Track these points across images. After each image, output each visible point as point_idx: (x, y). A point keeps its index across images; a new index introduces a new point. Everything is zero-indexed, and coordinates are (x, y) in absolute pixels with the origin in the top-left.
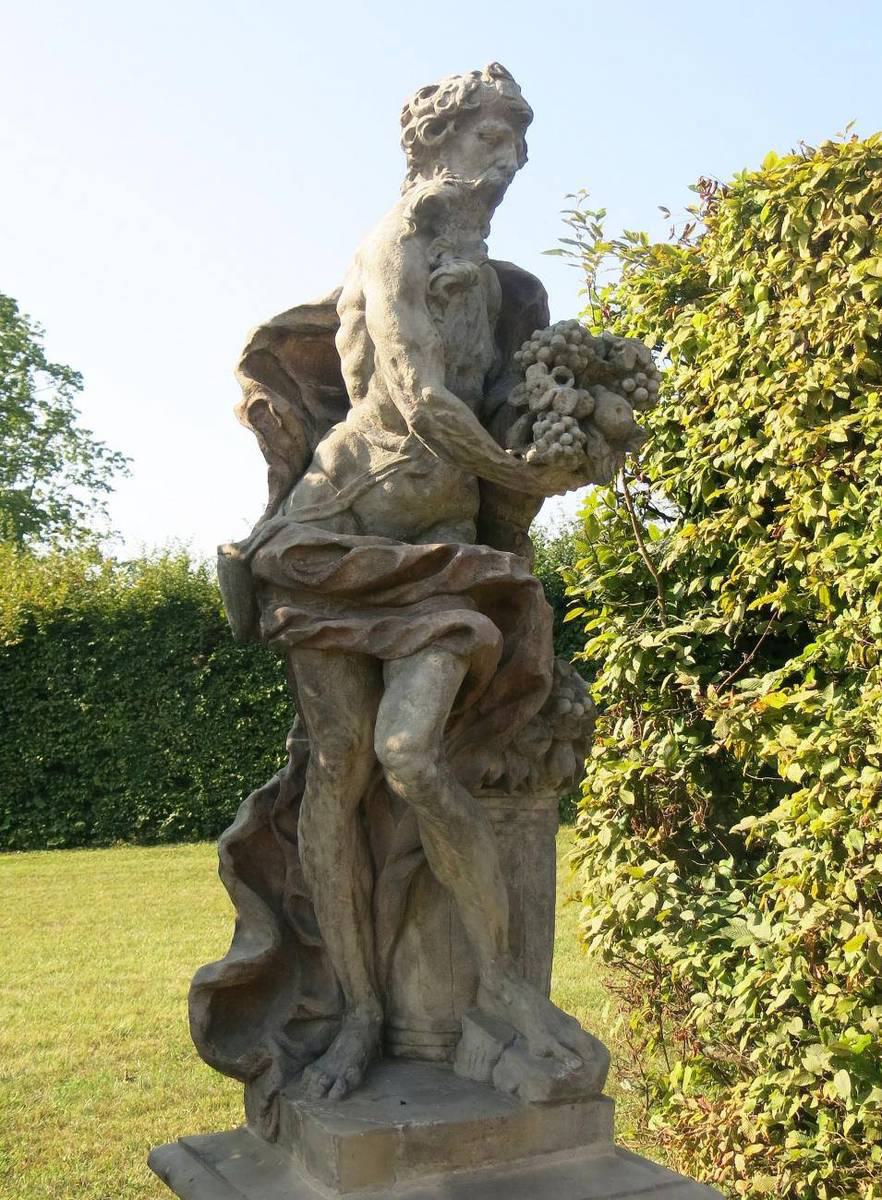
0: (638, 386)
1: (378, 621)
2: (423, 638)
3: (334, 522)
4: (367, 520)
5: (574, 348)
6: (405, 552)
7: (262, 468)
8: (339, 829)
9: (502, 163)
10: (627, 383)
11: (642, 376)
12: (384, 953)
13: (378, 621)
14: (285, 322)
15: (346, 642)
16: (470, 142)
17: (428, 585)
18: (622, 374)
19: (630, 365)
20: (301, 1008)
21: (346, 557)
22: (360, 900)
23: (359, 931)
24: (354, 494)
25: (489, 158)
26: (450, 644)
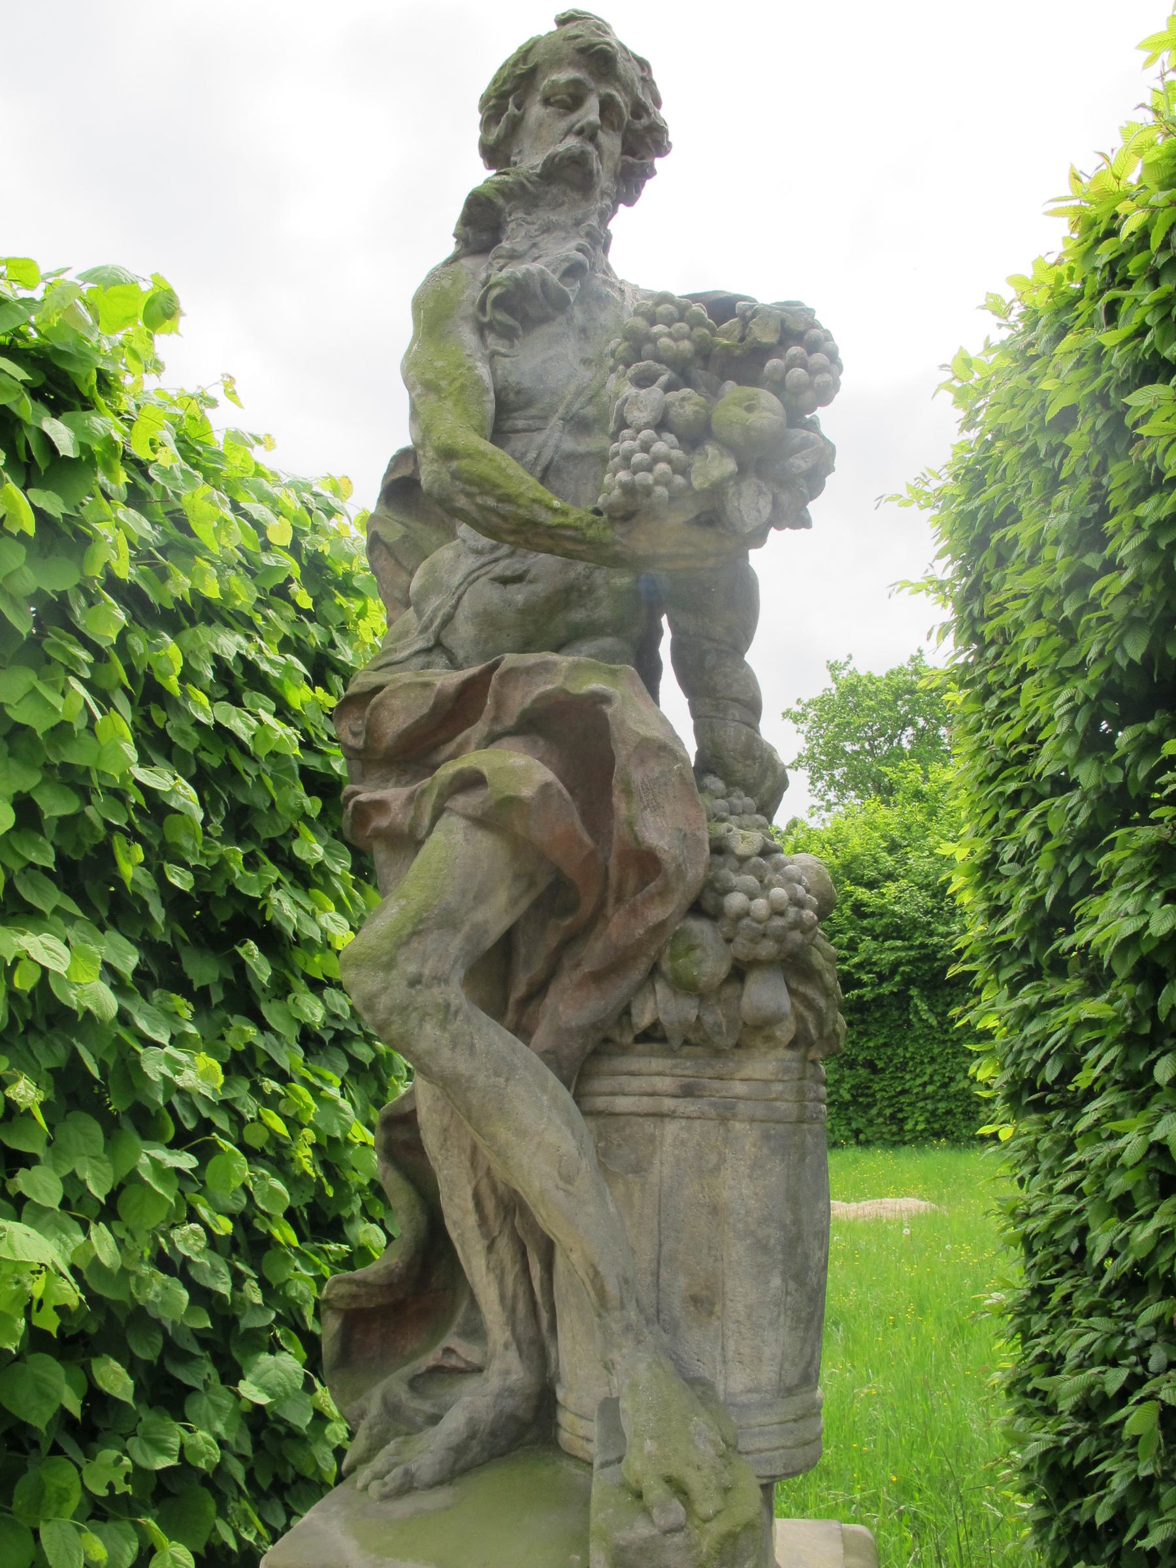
0: (788, 368)
10: (773, 363)
16: (536, 111)
18: (761, 353)
20: (448, 1351)
22: (490, 1205)
23: (490, 1248)
25: (563, 125)
26: (461, 802)
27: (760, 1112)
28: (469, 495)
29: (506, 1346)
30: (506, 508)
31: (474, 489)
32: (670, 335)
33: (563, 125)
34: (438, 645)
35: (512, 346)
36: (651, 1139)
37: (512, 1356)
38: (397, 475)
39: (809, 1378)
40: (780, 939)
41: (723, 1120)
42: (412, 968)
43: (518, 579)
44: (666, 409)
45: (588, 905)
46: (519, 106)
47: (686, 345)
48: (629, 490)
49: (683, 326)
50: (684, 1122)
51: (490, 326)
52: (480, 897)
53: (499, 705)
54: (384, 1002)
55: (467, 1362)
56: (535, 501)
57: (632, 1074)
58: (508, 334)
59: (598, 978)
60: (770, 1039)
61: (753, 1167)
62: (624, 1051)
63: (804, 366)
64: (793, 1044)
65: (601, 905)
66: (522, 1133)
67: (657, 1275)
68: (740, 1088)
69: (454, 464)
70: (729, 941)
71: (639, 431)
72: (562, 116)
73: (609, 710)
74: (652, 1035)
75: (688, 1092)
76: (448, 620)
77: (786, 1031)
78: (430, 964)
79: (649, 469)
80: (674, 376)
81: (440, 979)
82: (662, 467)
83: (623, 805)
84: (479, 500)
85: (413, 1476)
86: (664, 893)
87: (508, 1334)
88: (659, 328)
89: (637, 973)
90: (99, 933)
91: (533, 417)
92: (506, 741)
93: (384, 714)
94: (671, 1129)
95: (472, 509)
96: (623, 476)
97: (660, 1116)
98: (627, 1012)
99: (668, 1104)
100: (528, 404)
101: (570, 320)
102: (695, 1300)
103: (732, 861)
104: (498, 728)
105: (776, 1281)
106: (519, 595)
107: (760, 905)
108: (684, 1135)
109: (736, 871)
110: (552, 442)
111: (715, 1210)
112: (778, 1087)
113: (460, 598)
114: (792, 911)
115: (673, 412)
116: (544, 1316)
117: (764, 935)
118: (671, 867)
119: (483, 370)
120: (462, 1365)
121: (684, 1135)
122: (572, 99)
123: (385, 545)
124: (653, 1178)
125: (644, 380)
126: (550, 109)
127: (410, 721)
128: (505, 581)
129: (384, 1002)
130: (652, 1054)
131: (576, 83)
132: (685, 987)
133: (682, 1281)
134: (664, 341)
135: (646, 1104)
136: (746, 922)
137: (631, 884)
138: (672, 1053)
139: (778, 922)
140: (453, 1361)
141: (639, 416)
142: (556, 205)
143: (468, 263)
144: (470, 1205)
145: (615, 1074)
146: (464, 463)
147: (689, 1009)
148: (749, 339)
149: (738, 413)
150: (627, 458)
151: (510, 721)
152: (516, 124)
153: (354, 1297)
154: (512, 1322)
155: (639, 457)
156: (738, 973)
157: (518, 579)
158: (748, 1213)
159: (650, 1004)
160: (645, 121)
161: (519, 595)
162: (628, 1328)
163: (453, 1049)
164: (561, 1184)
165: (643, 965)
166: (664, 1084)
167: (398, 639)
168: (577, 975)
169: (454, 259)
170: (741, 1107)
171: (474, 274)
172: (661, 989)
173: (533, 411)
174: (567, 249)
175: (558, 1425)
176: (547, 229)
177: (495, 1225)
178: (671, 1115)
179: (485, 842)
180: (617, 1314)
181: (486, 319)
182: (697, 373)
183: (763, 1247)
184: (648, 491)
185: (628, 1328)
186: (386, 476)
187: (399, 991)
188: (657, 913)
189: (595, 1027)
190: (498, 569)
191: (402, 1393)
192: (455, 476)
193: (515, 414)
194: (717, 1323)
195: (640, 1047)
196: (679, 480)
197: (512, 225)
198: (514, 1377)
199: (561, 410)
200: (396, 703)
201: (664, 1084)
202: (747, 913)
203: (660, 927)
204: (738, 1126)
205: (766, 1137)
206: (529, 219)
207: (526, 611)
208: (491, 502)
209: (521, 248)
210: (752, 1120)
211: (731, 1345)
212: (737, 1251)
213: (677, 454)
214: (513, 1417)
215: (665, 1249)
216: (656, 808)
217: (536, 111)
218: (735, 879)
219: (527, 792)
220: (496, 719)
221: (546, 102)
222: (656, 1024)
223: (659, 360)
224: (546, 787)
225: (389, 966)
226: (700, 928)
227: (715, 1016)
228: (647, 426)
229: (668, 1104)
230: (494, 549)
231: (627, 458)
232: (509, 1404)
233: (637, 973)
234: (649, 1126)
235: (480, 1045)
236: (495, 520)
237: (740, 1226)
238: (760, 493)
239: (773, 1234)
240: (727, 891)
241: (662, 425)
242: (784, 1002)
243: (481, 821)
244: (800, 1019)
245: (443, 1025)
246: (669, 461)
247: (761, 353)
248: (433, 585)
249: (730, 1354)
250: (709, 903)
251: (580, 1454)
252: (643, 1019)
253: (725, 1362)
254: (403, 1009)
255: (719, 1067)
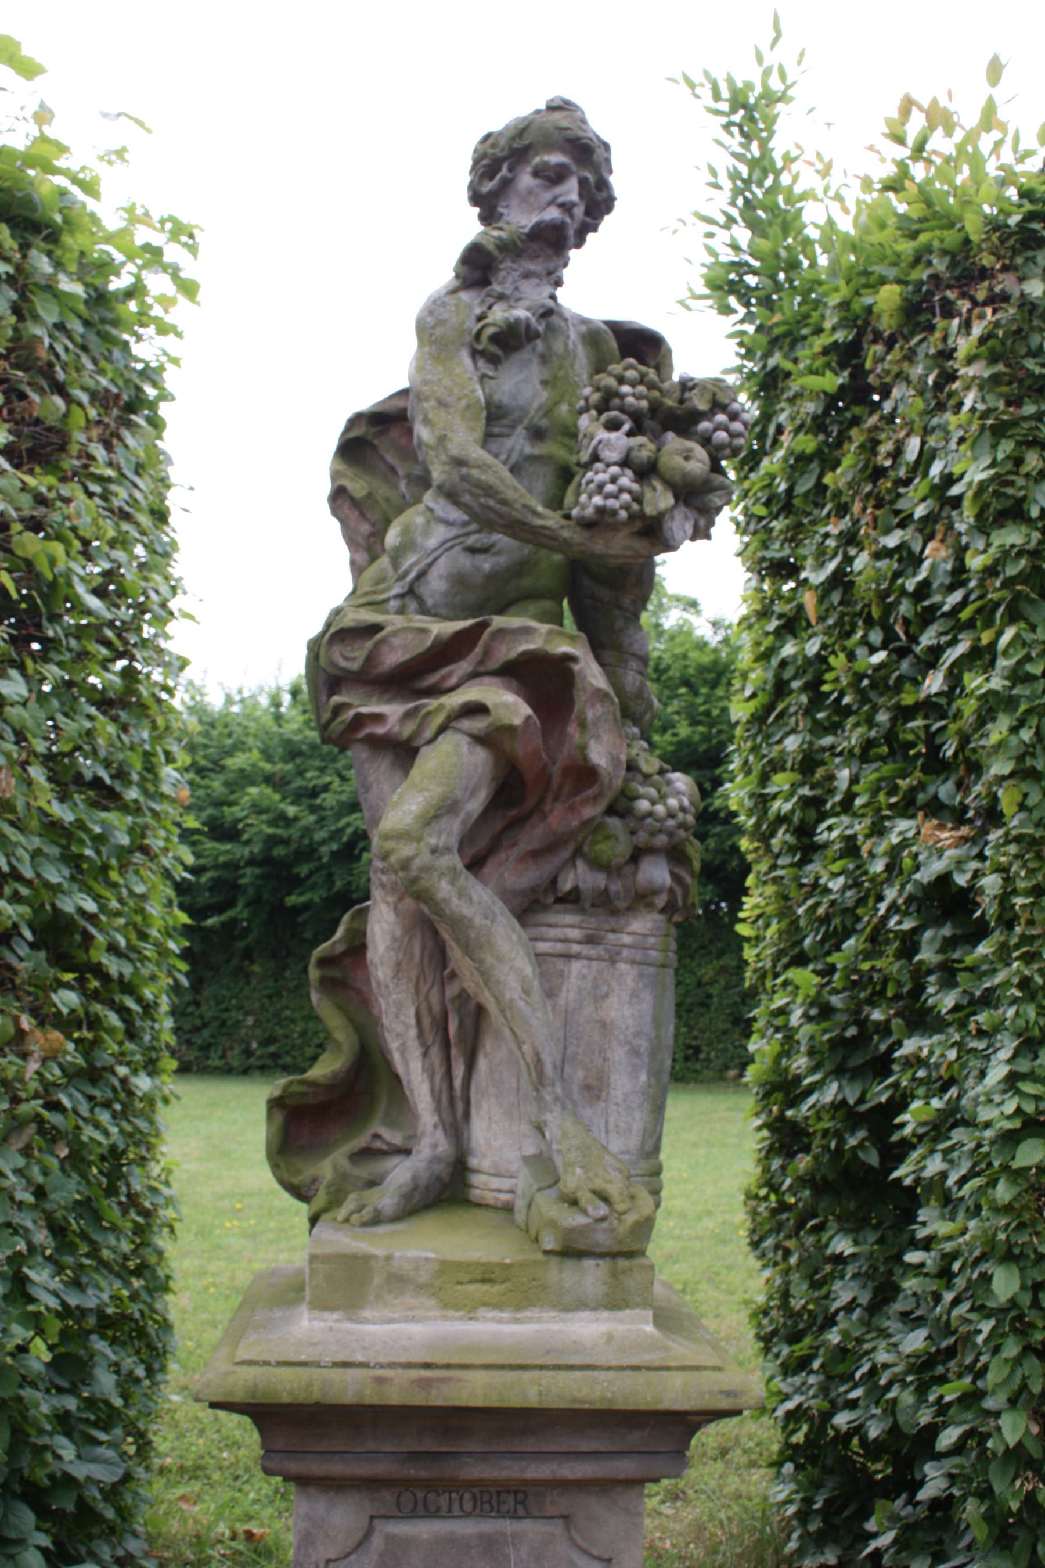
0: (715, 430)
1: (411, 705)
2: (439, 720)
3: (394, 604)
4: (430, 602)
5: (626, 389)
6: (780, 707)
7: (343, 554)
8: (394, 939)
9: (561, 200)
10: (704, 425)
11: (721, 418)
12: (458, 1083)
13: (411, 705)
14: (387, 407)
15: (380, 730)
16: (526, 180)
17: (464, 667)
18: (697, 416)
19: (702, 406)
20: (376, 1136)
21: (379, 636)
22: (427, 1021)
23: (425, 1054)
24: (412, 575)
25: (547, 196)
26: (466, 724)
27: (638, 955)
28: (472, 494)
29: (435, 1127)
30: (504, 509)
31: (479, 491)
32: (634, 395)
33: (547, 196)
34: (411, 592)
36: (561, 974)
37: (440, 1134)
38: (352, 435)
39: (657, 1149)
40: (671, 834)
41: (613, 961)
42: (433, 841)
43: (484, 550)
44: (629, 450)
45: (530, 802)
46: (510, 170)
47: (644, 404)
48: (601, 510)
49: (641, 389)
51: (483, 353)
52: (473, 793)
53: (487, 653)
54: (417, 863)
55: (388, 1144)
56: (525, 506)
57: (550, 926)
58: (494, 361)
59: (535, 855)
60: (650, 906)
62: (546, 908)
63: (726, 430)
64: (663, 911)
65: (541, 801)
66: (500, 959)
68: (627, 939)
69: (464, 470)
70: (633, 833)
71: (608, 466)
72: (547, 188)
73: (576, 667)
74: (572, 899)
75: (591, 940)
76: (422, 575)
77: (661, 901)
78: (443, 838)
79: (616, 497)
81: (448, 850)
82: (626, 497)
83: (577, 735)
84: (482, 500)
86: (596, 798)
87: (436, 1118)
88: (626, 389)
89: (566, 854)
92: (486, 680)
93: (385, 649)
94: (576, 966)
95: (475, 505)
96: (598, 500)
97: (568, 957)
98: (554, 882)
99: (576, 948)
100: (504, 416)
101: (534, 349)
102: (588, 1087)
104: (482, 669)
105: (643, 1078)
106: (487, 564)
107: (660, 809)
108: (585, 971)
109: (643, 784)
110: (518, 447)
111: (603, 1025)
112: (652, 940)
113: (436, 559)
114: (681, 815)
115: (634, 454)
116: (460, 1106)
117: (660, 831)
118: (606, 781)
119: (480, 393)
120: (385, 1147)
121: (585, 971)
122: (555, 176)
123: (352, 499)
124: (561, 1001)
125: (613, 426)
126: (538, 181)
127: (407, 656)
128: (473, 550)
129: (417, 863)
130: (566, 912)
131: (562, 166)
132: (597, 864)
133: (580, 1074)
134: (630, 400)
135: (560, 947)
136: (649, 820)
137: (567, 789)
138: (582, 911)
139: (671, 823)
140: (378, 1144)
141: (614, 456)
142: (534, 257)
143: (465, 296)
144: (413, 1021)
145: (536, 925)
146: (475, 473)
147: (600, 880)
148: (687, 404)
149: (679, 460)
150: (600, 487)
151: (494, 664)
152: (506, 184)
153: (304, 1094)
154: (438, 1109)
155: (610, 488)
156: (637, 855)
157: (484, 550)
159: (571, 876)
160: (604, 194)
162: (557, 1099)
165: (571, 848)
166: (574, 933)
167: (377, 583)
168: (515, 853)
169: (453, 292)
170: (625, 953)
171: (470, 308)
172: (581, 866)
173: (506, 422)
174: (536, 294)
175: (469, 1186)
176: (527, 275)
177: (429, 1037)
178: (577, 956)
179: (481, 756)
181: (480, 347)
182: (648, 423)
183: (635, 1052)
184: (614, 513)
185: (557, 1099)
186: (344, 434)
187: (425, 858)
188: (589, 812)
189: (534, 890)
190: (471, 541)
191: (345, 1164)
192: (464, 478)
195: (558, 907)
196: (635, 506)
197: (503, 273)
198: (441, 1149)
199: (526, 422)
200: (396, 641)
201: (574, 933)
202: (650, 814)
203: (591, 820)
204: (623, 967)
205: (641, 975)
207: (492, 577)
208: (492, 503)
209: (508, 292)
210: (633, 962)
211: (612, 1120)
212: (618, 1054)
213: (635, 487)
214: (438, 1178)
215: (569, 1051)
216: (598, 737)
217: (526, 180)
218: (642, 790)
219: (517, 721)
220: (481, 662)
221: (536, 174)
222: (576, 889)
223: (622, 410)
225: (419, 839)
226: (614, 823)
227: (615, 887)
228: (615, 464)
229: (576, 948)
230: (465, 524)
231: (600, 487)
232: (438, 1168)
233: (566, 854)
234: (560, 964)
235: (475, 897)
236: (492, 516)
238: (686, 518)
239: (644, 1045)
240: (637, 797)
241: (625, 463)
242: (668, 880)
243: (479, 739)
244: (671, 891)
245: (452, 882)
246: (630, 492)
247: (697, 416)
248: (408, 545)
249: (611, 1127)
250: (623, 803)
251: (492, 1202)
252: (567, 884)
255: (613, 922)
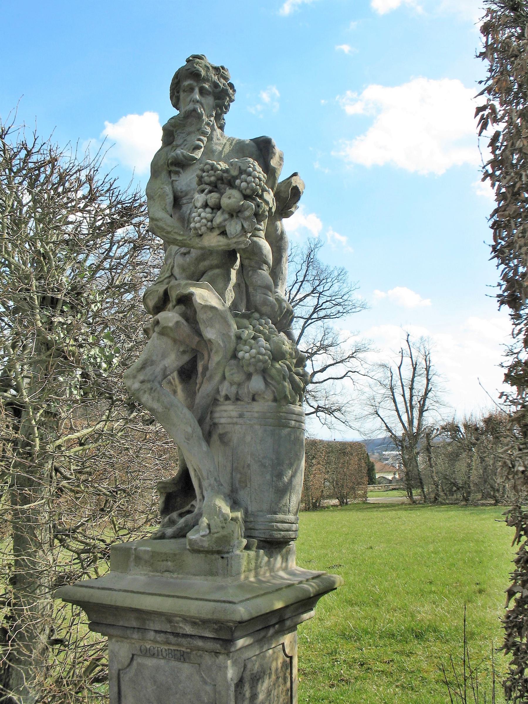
32: (207, 176)
35: (179, 177)
50: (240, 426)
61: (261, 441)
67: (232, 474)
79: (200, 222)
80: (211, 188)
85: (165, 534)
90: (229, 395)
91: (189, 199)
103: (242, 342)
105: (268, 477)
139: (253, 360)
158: (259, 455)
161: (188, 259)
163: (153, 401)
164: (186, 440)
166: (234, 414)
176: (189, 134)
180: (207, 481)
183: (263, 466)
193: (183, 199)
194: (249, 489)
196: (209, 223)
205: (265, 431)
206: (183, 132)
215: (234, 466)
219: (171, 324)
224: (177, 323)
225: (135, 377)
237: (256, 459)
246: (206, 218)
253: (251, 502)
254: (138, 390)
